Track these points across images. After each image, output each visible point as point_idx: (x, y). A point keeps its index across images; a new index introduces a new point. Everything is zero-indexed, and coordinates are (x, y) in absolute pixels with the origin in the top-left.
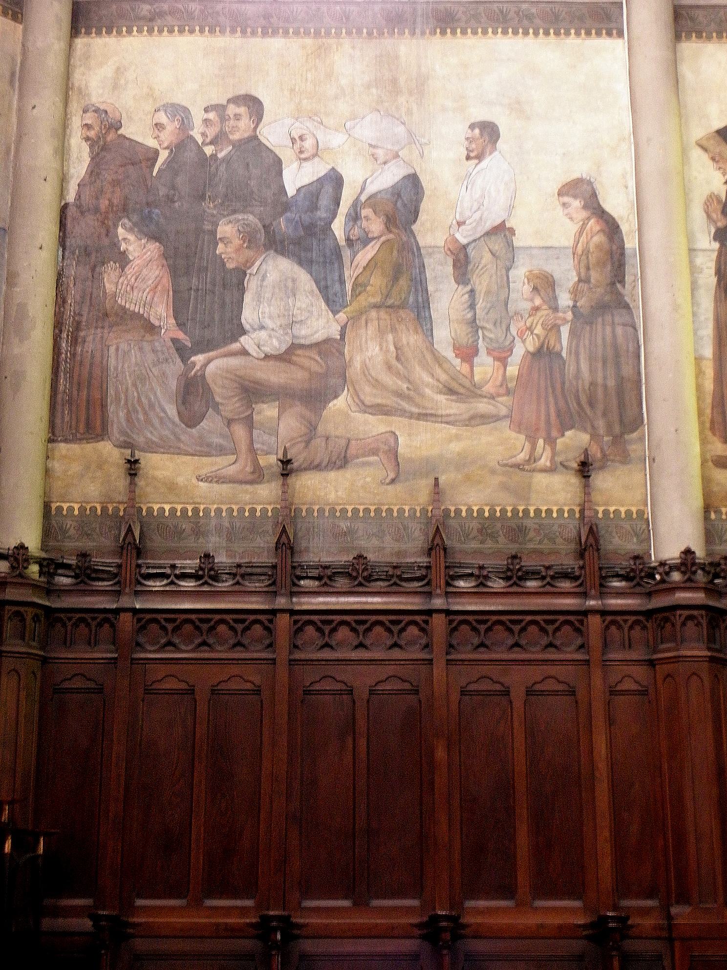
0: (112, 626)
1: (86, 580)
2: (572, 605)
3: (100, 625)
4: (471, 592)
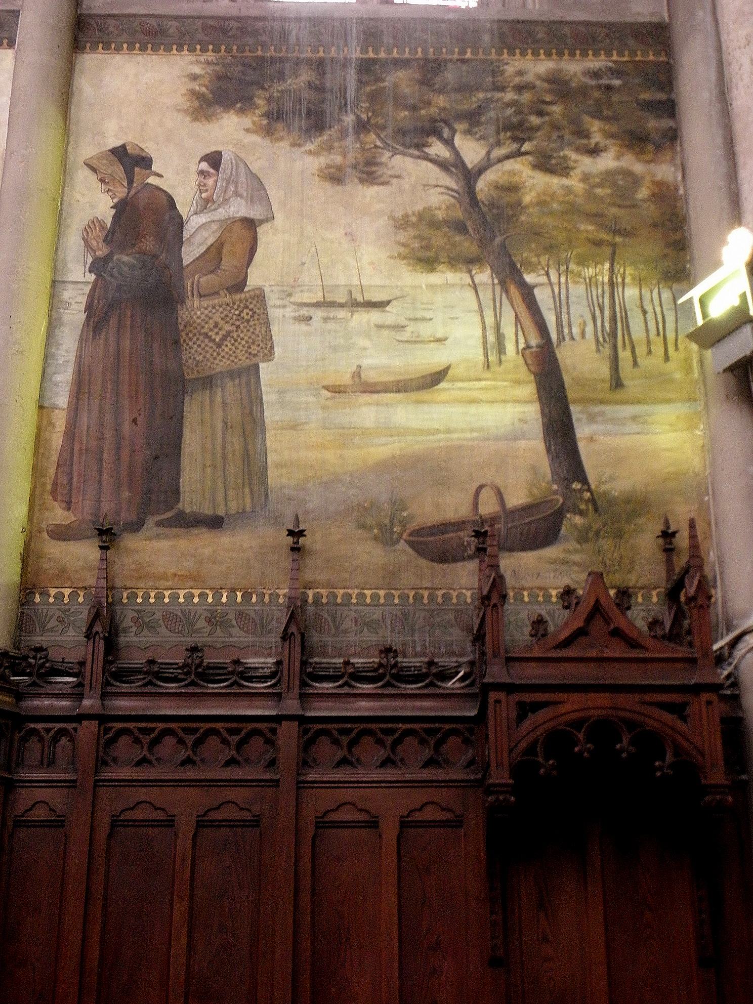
0: (72, 740)
1: (154, 680)
2: (62, 708)
3: (55, 740)
4: (335, 694)
